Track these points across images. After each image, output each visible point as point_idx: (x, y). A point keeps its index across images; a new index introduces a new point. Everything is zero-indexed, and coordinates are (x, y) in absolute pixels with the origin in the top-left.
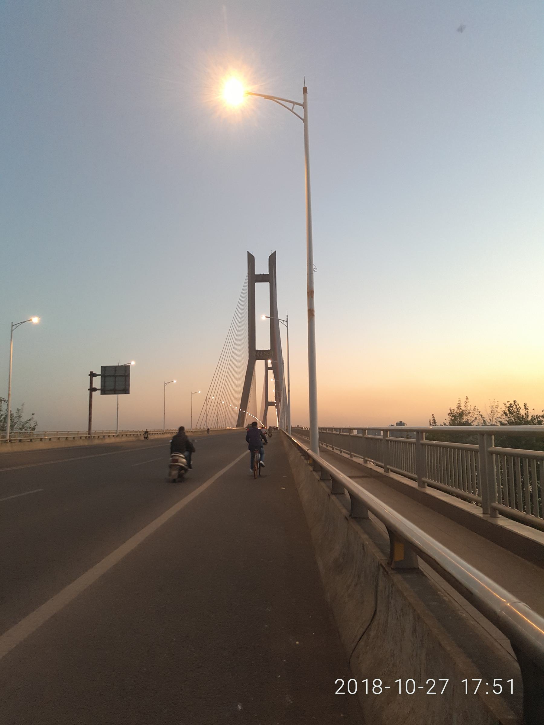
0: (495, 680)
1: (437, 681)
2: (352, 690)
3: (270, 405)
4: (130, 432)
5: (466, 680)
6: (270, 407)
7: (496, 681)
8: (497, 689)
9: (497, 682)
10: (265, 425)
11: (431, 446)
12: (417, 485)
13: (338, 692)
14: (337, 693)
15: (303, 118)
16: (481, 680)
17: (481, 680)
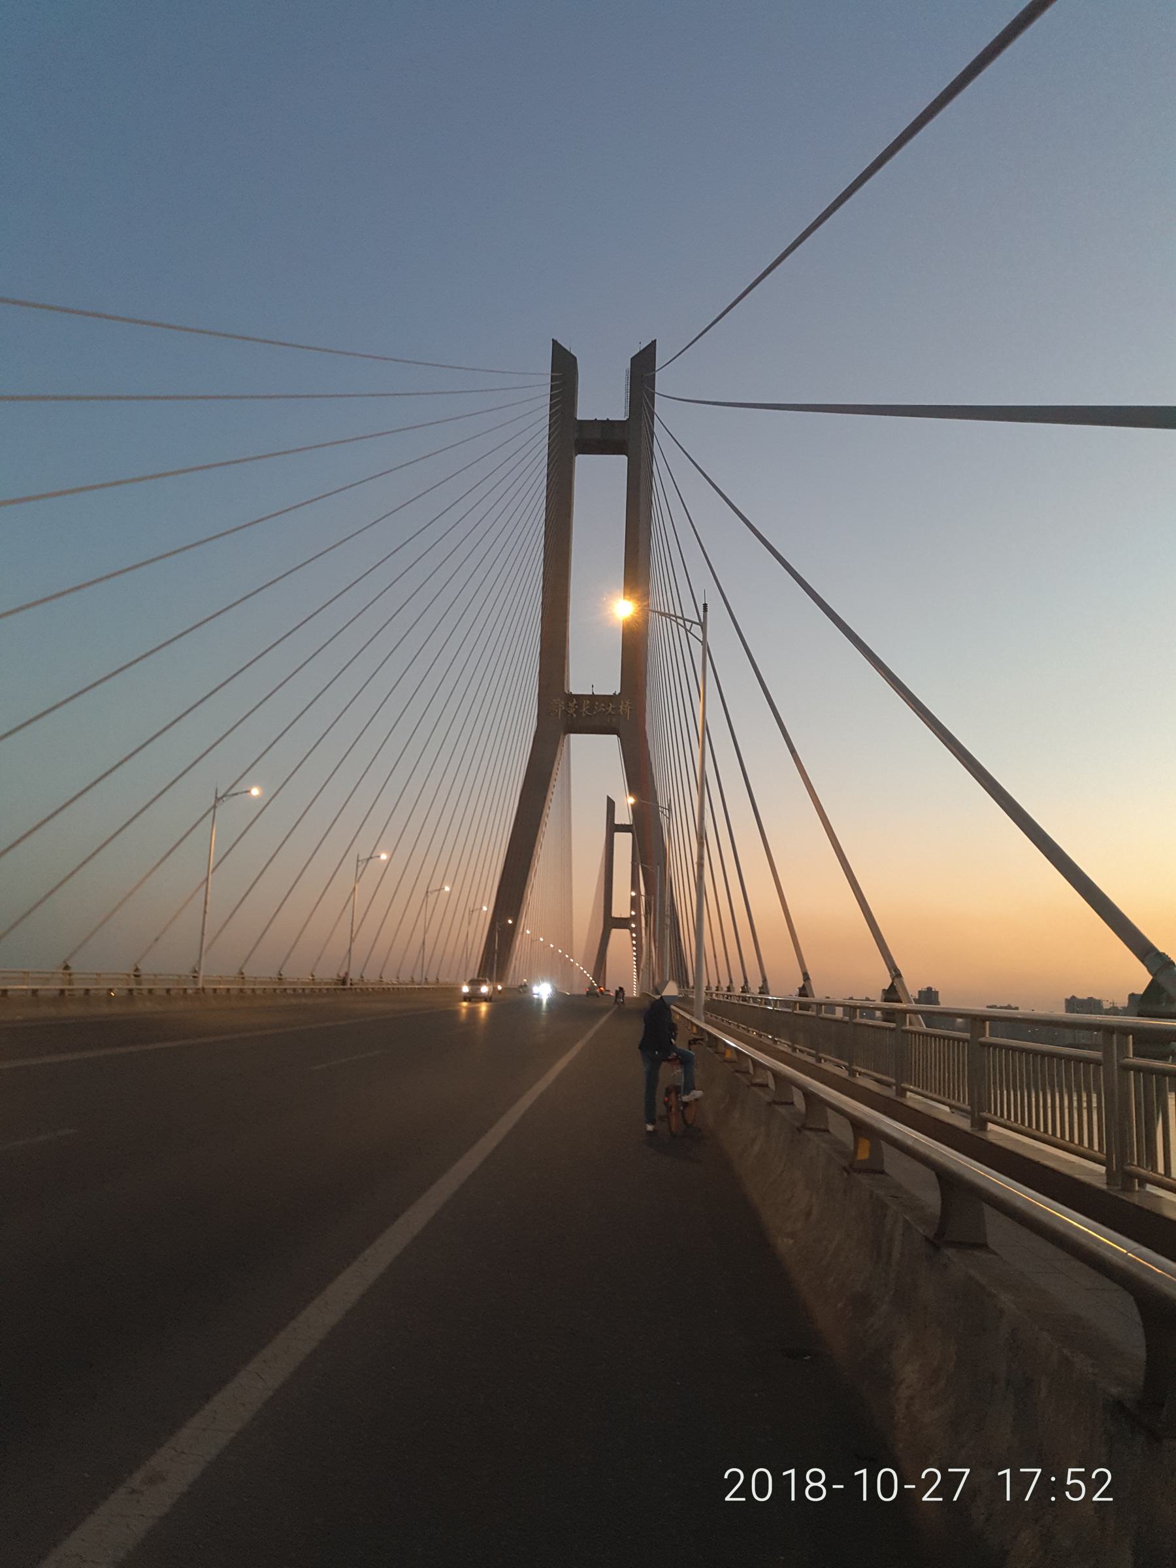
0: (1070, 1470)
1: (945, 1474)
2: (762, 1492)
3: (615, 928)
4: (302, 982)
5: (1008, 1471)
6: (615, 932)
7: (1072, 1473)
8: (1075, 1490)
9: (1075, 1476)
10: (601, 980)
11: (964, 1042)
12: (969, 1125)
13: (732, 1497)
14: (728, 1498)
15: (702, 640)
16: (1039, 1471)
17: (1039, 1471)
